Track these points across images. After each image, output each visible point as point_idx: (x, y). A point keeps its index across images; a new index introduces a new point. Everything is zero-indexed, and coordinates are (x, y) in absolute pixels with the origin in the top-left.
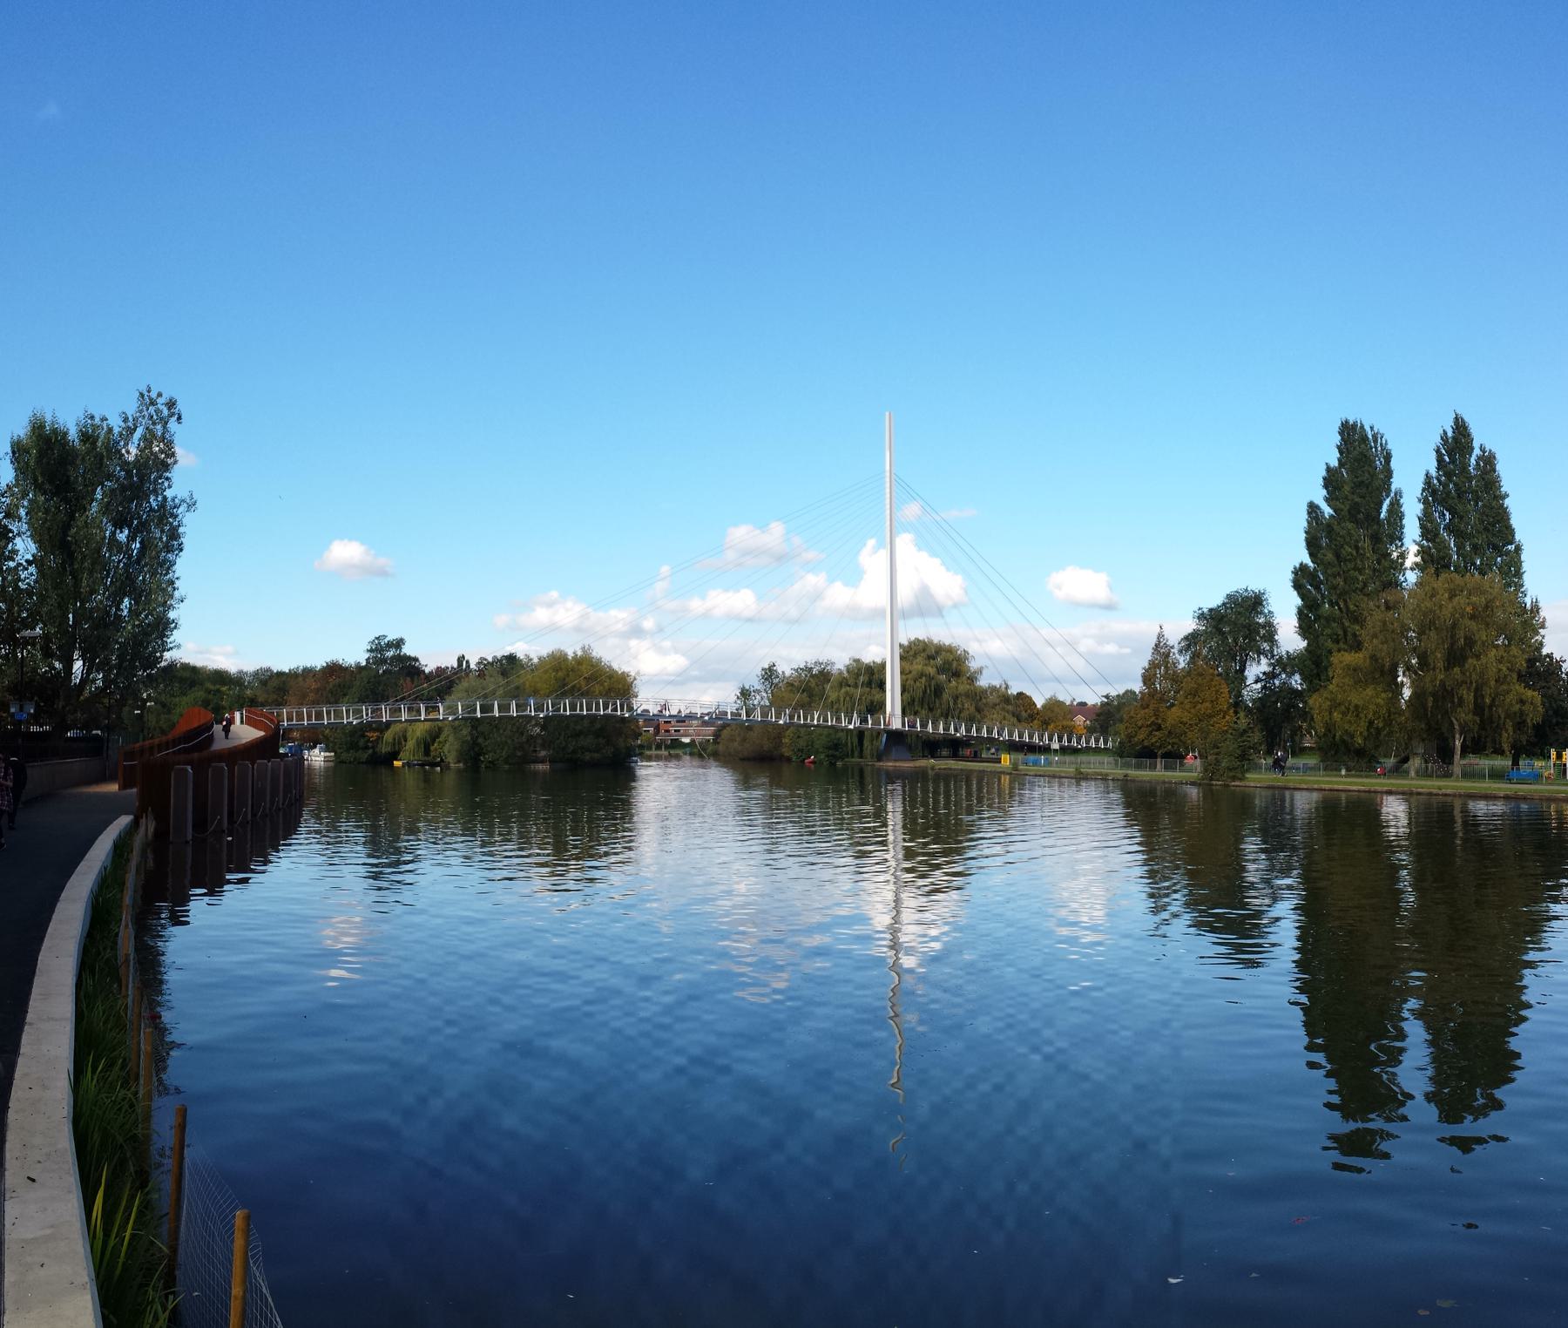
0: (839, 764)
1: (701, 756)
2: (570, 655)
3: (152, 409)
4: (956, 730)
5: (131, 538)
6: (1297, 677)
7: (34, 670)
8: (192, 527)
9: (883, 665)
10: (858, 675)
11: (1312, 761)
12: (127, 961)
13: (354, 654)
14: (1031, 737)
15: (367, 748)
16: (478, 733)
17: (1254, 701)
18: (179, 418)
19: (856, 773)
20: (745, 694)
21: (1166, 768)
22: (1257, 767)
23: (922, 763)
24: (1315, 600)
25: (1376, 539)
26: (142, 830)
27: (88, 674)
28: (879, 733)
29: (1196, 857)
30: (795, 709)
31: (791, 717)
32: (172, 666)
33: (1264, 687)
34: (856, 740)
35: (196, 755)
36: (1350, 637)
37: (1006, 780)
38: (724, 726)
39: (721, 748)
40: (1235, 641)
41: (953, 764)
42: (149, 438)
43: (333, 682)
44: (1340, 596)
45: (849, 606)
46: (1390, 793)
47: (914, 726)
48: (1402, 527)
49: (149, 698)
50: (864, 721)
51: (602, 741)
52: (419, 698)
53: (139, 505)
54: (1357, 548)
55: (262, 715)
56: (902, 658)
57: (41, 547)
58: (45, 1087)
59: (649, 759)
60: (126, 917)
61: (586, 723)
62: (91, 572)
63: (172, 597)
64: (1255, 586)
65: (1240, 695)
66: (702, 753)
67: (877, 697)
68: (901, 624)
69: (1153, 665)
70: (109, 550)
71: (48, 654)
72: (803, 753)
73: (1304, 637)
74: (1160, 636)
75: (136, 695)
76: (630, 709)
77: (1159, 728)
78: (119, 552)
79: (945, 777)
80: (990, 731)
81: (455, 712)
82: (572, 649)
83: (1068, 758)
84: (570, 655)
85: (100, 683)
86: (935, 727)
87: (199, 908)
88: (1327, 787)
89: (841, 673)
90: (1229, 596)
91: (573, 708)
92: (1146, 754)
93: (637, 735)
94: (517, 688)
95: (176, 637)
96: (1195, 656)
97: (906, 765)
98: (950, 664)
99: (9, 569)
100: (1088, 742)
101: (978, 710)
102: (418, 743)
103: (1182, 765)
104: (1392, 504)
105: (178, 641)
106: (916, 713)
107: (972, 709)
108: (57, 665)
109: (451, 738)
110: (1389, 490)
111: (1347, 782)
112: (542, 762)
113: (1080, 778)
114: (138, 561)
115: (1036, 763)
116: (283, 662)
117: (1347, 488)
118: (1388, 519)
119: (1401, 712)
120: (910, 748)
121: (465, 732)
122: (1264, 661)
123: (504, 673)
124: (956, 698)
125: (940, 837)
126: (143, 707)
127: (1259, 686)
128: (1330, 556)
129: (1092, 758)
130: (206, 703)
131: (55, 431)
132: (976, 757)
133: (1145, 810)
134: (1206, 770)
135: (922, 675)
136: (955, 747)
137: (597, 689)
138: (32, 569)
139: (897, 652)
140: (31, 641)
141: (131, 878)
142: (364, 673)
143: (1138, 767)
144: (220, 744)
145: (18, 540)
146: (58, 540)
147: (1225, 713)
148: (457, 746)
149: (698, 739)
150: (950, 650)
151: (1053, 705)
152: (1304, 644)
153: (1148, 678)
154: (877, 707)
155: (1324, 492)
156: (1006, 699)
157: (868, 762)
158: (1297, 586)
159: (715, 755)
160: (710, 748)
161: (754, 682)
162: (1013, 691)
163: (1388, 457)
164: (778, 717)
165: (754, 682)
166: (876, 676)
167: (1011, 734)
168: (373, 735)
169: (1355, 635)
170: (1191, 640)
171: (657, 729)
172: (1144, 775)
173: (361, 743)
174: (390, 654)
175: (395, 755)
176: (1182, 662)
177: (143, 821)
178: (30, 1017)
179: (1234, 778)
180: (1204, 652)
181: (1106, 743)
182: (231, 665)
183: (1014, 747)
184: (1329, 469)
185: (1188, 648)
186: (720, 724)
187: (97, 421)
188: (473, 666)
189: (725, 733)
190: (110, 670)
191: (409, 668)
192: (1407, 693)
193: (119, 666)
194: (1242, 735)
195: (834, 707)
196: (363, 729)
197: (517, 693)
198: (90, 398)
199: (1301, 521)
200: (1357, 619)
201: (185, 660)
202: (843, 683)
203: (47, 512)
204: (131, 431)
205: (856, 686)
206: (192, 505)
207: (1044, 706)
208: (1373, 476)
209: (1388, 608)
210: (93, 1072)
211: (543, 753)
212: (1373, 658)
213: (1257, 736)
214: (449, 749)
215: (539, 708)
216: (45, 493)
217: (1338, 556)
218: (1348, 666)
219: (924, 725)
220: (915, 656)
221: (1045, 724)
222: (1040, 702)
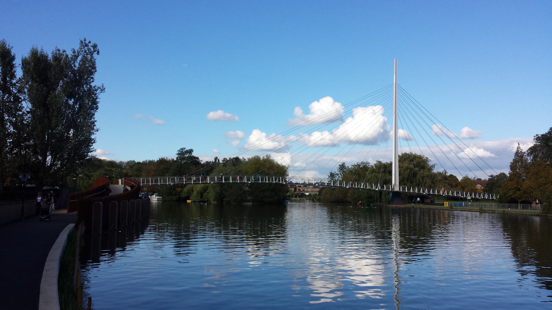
0: (372, 205)
1: (313, 201)
2: (262, 158)
3: (86, 48)
4: (423, 191)
5: (75, 103)
7: (29, 159)
8: (102, 99)
9: (391, 164)
13: (172, 155)
15: (176, 195)
16: (223, 189)
18: (98, 52)
20: (332, 175)
21: (523, 208)
23: (409, 205)
27: (54, 161)
28: (389, 192)
31: (352, 185)
34: (378, 195)
38: (323, 188)
39: (322, 197)
42: (84, 60)
43: (162, 166)
50: (382, 187)
53: (79, 89)
55: (132, 181)
56: (399, 161)
59: (292, 201)
63: (93, 129)
66: (313, 199)
67: (388, 177)
69: (515, 161)
70: (65, 108)
71: (36, 153)
76: (285, 181)
78: (69, 109)
80: (438, 192)
81: (214, 180)
82: (262, 156)
83: (475, 204)
84: (262, 158)
86: (414, 190)
89: (372, 167)
91: (262, 180)
92: (513, 202)
93: (288, 191)
94: (240, 171)
95: (94, 146)
96: (535, 157)
98: (420, 163)
99: (19, 115)
101: (433, 183)
102: (198, 193)
103: (531, 207)
106: (405, 184)
107: (430, 182)
108: (40, 158)
109: (212, 191)
112: (249, 201)
113: (482, 211)
114: (78, 113)
116: (140, 159)
121: (217, 189)
123: (234, 165)
125: (417, 238)
129: (488, 204)
131: (42, 55)
132: (432, 203)
133: (513, 228)
134: (544, 209)
135: (407, 169)
138: (29, 115)
145: (23, 103)
146: (41, 103)
150: (420, 157)
151: (466, 180)
153: (513, 167)
159: (319, 200)
161: (336, 170)
162: (448, 174)
164: (346, 185)
165: (336, 170)
166: (388, 169)
168: (179, 189)
170: (532, 150)
171: (295, 189)
176: (529, 159)
183: (448, 198)
187: (61, 52)
188: (221, 162)
189: (324, 191)
190: (64, 160)
191: (195, 161)
195: (370, 181)
196: (175, 186)
197: (239, 172)
198: (57, 40)
203: (37, 90)
204: (77, 57)
206: (103, 90)
207: (462, 180)
211: (249, 198)
214: (211, 195)
215: (248, 180)
216: (36, 82)
219: (409, 189)
220: (405, 160)
222: (460, 178)
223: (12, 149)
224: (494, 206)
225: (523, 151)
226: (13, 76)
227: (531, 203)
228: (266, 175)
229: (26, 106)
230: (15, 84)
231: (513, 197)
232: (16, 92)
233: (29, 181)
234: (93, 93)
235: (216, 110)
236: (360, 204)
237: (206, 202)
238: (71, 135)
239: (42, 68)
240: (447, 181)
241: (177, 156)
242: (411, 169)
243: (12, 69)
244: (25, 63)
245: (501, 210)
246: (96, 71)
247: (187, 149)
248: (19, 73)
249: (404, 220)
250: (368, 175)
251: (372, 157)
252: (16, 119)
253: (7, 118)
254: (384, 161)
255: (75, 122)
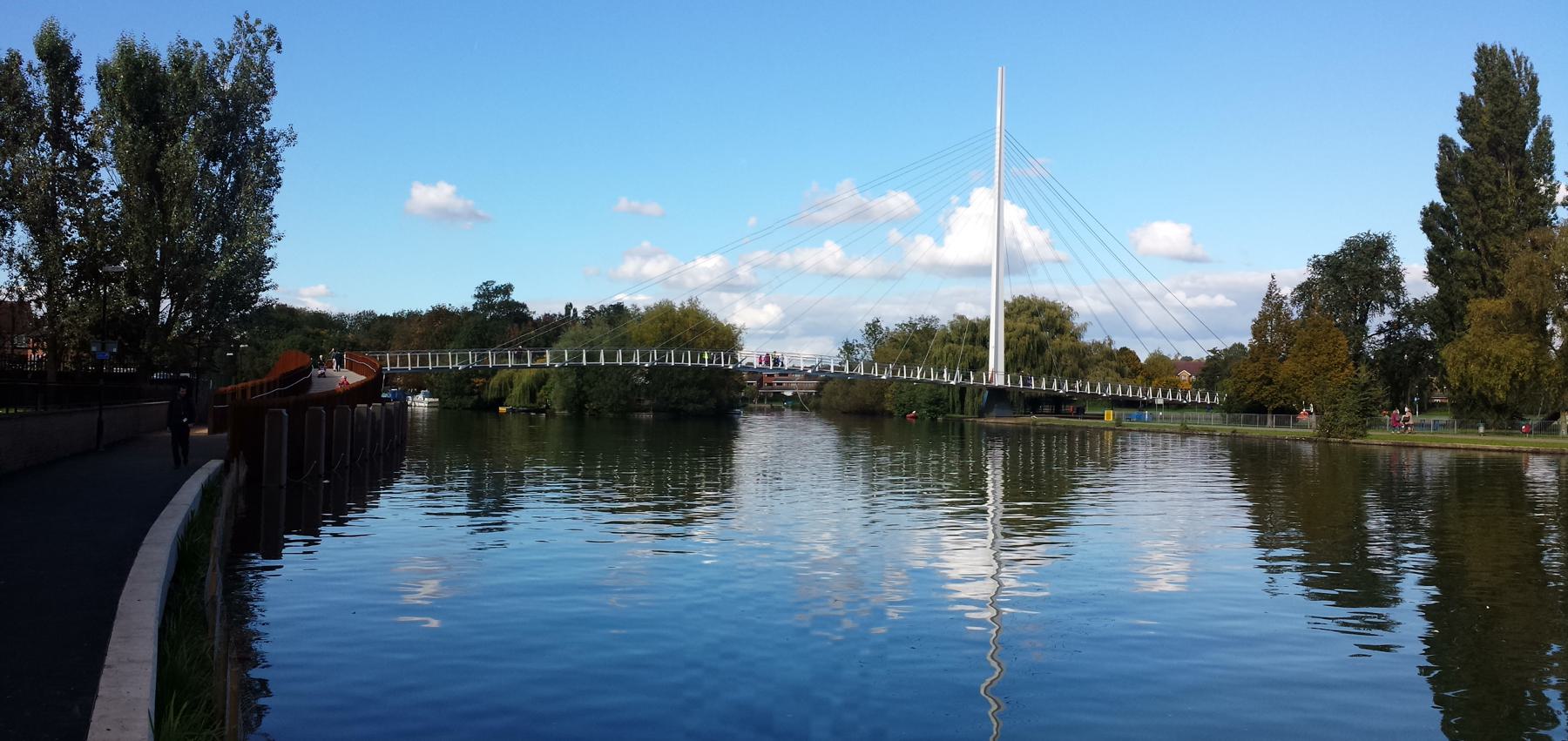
1: (802, 409)
2: (678, 306)
3: (250, 36)
5: (225, 171)
6: (1427, 327)
8: (290, 162)
9: (987, 323)
10: (962, 332)
11: (1444, 419)
12: (214, 604)
13: (462, 299)
14: (1135, 392)
15: (472, 394)
16: (583, 382)
17: (1376, 353)
18: (279, 47)
19: (957, 430)
20: (848, 348)
21: (1278, 424)
22: (1379, 425)
24: (1448, 242)
25: (1520, 173)
26: (233, 474)
28: (981, 390)
29: (1313, 516)
30: (899, 364)
31: (895, 372)
32: (267, 308)
33: (1387, 339)
35: (292, 398)
36: (1488, 282)
37: (1109, 436)
38: (827, 380)
39: (823, 401)
40: (1355, 289)
41: (1054, 420)
42: (244, 70)
43: (439, 327)
44: (1477, 237)
45: (954, 249)
46: (1537, 453)
47: (1017, 382)
48: (1552, 158)
49: (243, 340)
50: (967, 377)
51: (706, 392)
52: (526, 345)
53: (235, 137)
54: (1498, 183)
55: (364, 359)
56: (1007, 315)
57: (127, 178)
58: (124, 729)
59: (752, 411)
60: (214, 560)
61: (690, 375)
62: (181, 205)
64: (1378, 230)
65: (1360, 346)
66: (802, 405)
68: (1004, 280)
69: (1264, 317)
70: (202, 183)
72: (905, 407)
73: (1436, 283)
74: (1272, 286)
75: (228, 336)
76: (735, 361)
77: (1270, 382)
79: (1049, 432)
80: (1093, 388)
81: (561, 359)
82: (679, 301)
83: (1172, 414)
84: (678, 306)
85: (189, 323)
86: (1038, 383)
87: (293, 549)
88: (1462, 445)
89: (945, 329)
90: (1348, 242)
91: (678, 359)
92: (1257, 410)
93: (741, 388)
94: (624, 337)
95: (272, 276)
97: (1009, 422)
99: (93, 201)
100: (1193, 397)
101: (1082, 366)
102: (524, 390)
103: (1295, 420)
104: (1539, 133)
105: (275, 281)
108: (143, 303)
109: (557, 385)
110: (1535, 118)
111: (1485, 442)
112: (646, 411)
113: (1186, 433)
114: (232, 196)
115: (1140, 419)
116: (386, 307)
117: (1485, 119)
118: (1534, 150)
119: (1550, 364)
120: (1012, 405)
121: (570, 380)
122: (1388, 310)
123: (611, 322)
124: (1059, 355)
125: (1041, 497)
126: (236, 350)
127: (1382, 336)
128: (1466, 194)
130: (304, 347)
131: (145, 55)
132: (1080, 412)
133: (1255, 469)
136: (1057, 403)
137: (702, 341)
138: (117, 201)
139: (1002, 309)
140: (117, 277)
141: (220, 522)
142: (471, 319)
143: (1247, 422)
144: (318, 388)
145: (102, 170)
146: (147, 173)
147: (1344, 366)
148: (562, 393)
149: (800, 392)
150: (1054, 307)
151: (1158, 360)
152: (1436, 290)
153: (1258, 330)
154: (979, 364)
155: (1459, 124)
156: (1110, 355)
157: (970, 420)
158: (1427, 228)
159: (817, 408)
160: (812, 402)
161: (858, 337)
162: (1117, 347)
163: (1534, 82)
164: (881, 372)
165: (858, 337)
166: (979, 334)
167: (1114, 390)
168: (479, 381)
169: (1495, 280)
170: (1305, 290)
171: (760, 381)
172: (1254, 431)
173: (467, 387)
174: (498, 299)
175: (500, 401)
176: (1296, 313)
177: (234, 466)
178: (109, 660)
179: (1354, 435)
180: (1321, 301)
181: (1212, 398)
182: (332, 308)
183: (1117, 403)
184: (1464, 99)
185: (1301, 298)
186: (821, 378)
187: (191, 47)
188: (580, 315)
189: (828, 387)
191: (517, 314)
192: (1557, 342)
193: (210, 305)
194: (1363, 389)
196: (469, 374)
197: (624, 342)
199: (1432, 156)
200: (1498, 262)
201: (282, 301)
202: (946, 339)
203: (134, 140)
204: (227, 59)
205: (959, 343)
206: (291, 139)
208: (1517, 104)
209: (1536, 248)
210: (175, 715)
211: (647, 403)
212: (1518, 304)
213: (1379, 391)
214: (555, 395)
215: (644, 358)
216: (132, 121)
217: (1474, 192)
218: (1488, 314)
220: (1019, 313)
221: (1149, 379)
222: (1143, 357)
223: (77, 284)
224: (1214, 421)
225: (1283, 293)
226: (76, 106)
227: (1297, 413)
228: (688, 346)
229: (110, 178)
230: (81, 126)
231: (1256, 398)
232: (84, 144)
233: (120, 359)
234: (269, 148)
235: (431, 181)
236: (915, 417)
237: (543, 411)
238: (218, 249)
239: (145, 89)
240: (1114, 363)
241: (474, 301)
242: (1033, 335)
243: (73, 89)
244: (105, 76)
245: (1227, 429)
246: (274, 93)
247: (499, 283)
248: (91, 98)
249: (1014, 454)
250: (935, 349)
251: (944, 306)
252: (86, 211)
253: (63, 208)
254: (971, 316)
255: (227, 217)
